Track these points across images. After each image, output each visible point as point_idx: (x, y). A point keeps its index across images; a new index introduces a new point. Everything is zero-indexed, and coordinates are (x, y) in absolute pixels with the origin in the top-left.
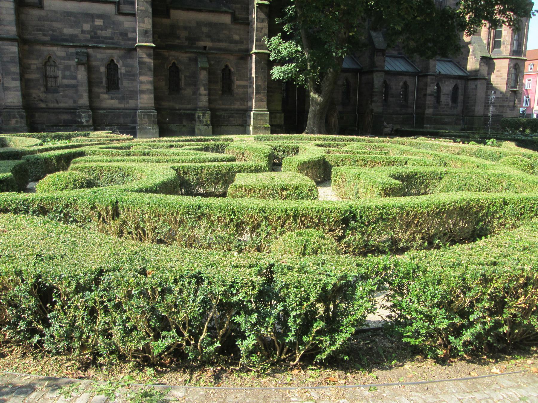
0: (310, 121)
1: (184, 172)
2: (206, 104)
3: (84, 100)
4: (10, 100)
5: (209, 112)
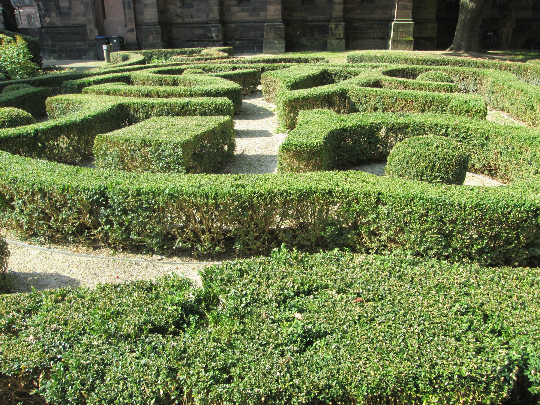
0: (457, 34)
1: (134, 110)
2: (341, 14)
3: (215, 14)
4: (149, 17)
5: (343, 23)
